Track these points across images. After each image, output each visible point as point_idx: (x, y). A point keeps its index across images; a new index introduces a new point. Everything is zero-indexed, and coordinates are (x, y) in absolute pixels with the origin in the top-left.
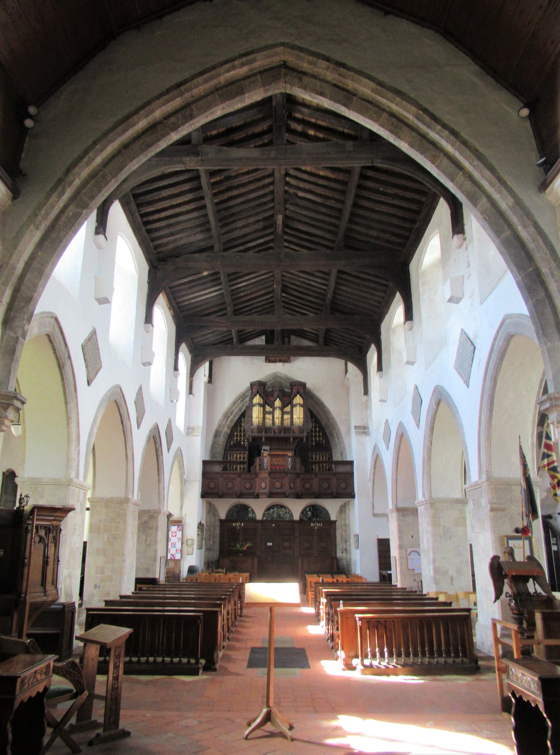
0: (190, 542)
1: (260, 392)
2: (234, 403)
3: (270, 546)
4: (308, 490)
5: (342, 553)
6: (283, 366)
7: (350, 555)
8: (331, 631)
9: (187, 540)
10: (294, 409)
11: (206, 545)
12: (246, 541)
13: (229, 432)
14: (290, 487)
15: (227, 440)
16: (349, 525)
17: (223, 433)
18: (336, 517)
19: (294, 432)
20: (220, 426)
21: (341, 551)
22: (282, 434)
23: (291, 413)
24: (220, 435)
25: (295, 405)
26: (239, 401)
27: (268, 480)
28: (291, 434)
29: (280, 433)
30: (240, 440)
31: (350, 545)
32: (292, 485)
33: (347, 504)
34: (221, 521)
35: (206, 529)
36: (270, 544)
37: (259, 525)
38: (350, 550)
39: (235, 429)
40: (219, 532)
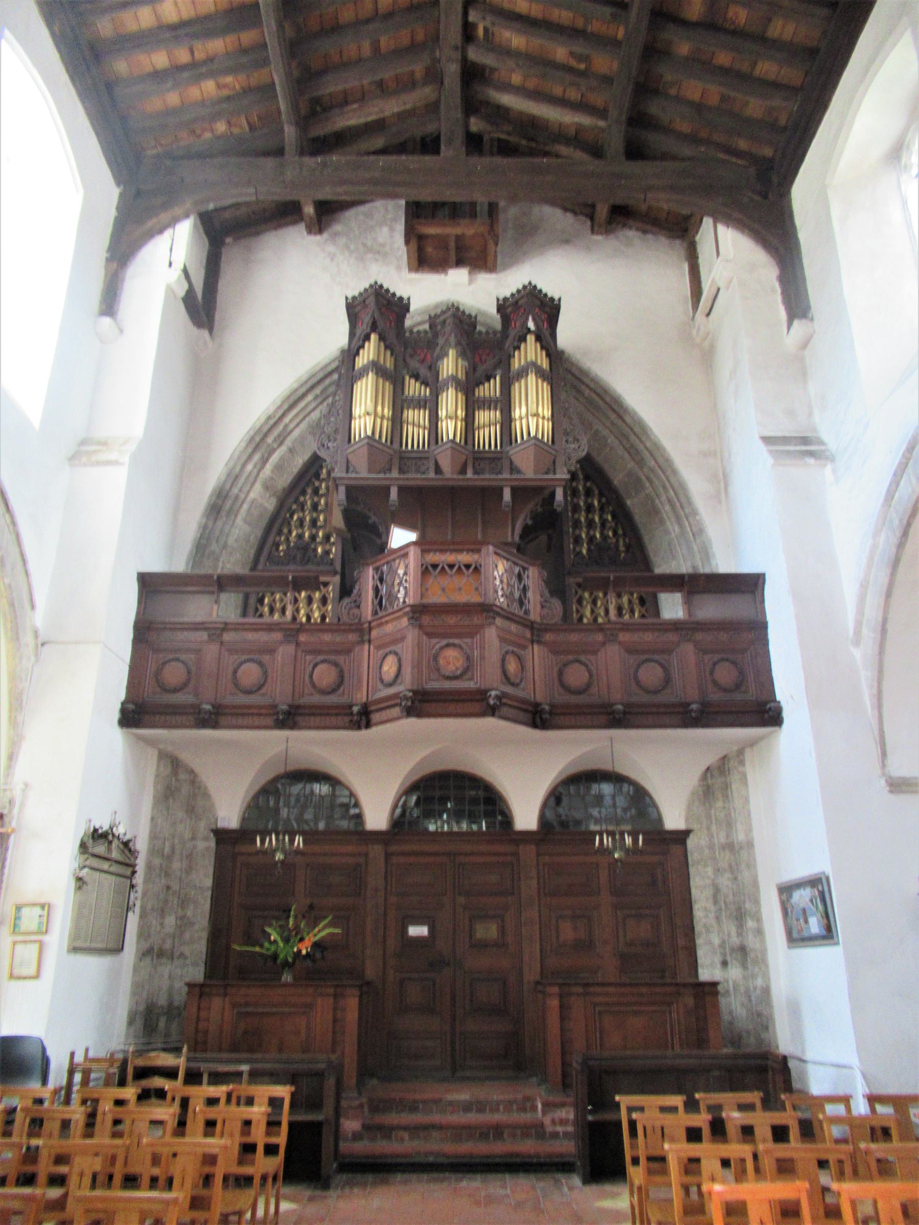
0: (30, 919)
1: (381, 324)
2: (293, 401)
3: (419, 940)
4: (579, 692)
5: (725, 964)
6: (471, 282)
7: (766, 976)
8: (219, 524)
9: (19, 908)
10: (517, 389)
11: (143, 934)
12: (312, 915)
13: (270, 505)
14: (505, 673)
15: (259, 533)
16: (750, 845)
17: (245, 506)
18: (687, 819)
19: (513, 469)
20: (233, 477)
21: (718, 959)
22: (470, 474)
23: (505, 404)
24: (233, 512)
25: (522, 373)
26: (310, 397)
27: (407, 649)
28: (506, 475)
29: (463, 471)
30: (313, 538)
31: (759, 932)
32: (512, 666)
33: (732, 763)
34: (222, 836)
35: (149, 867)
36: (418, 931)
37: (376, 851)
38: (764, 951)
39: (296, 501)
40: (209, 882)
